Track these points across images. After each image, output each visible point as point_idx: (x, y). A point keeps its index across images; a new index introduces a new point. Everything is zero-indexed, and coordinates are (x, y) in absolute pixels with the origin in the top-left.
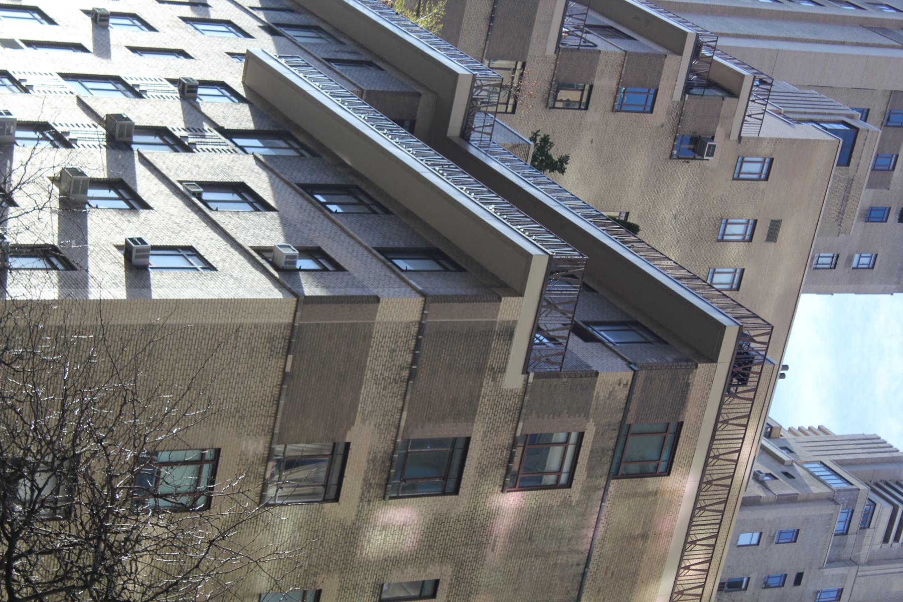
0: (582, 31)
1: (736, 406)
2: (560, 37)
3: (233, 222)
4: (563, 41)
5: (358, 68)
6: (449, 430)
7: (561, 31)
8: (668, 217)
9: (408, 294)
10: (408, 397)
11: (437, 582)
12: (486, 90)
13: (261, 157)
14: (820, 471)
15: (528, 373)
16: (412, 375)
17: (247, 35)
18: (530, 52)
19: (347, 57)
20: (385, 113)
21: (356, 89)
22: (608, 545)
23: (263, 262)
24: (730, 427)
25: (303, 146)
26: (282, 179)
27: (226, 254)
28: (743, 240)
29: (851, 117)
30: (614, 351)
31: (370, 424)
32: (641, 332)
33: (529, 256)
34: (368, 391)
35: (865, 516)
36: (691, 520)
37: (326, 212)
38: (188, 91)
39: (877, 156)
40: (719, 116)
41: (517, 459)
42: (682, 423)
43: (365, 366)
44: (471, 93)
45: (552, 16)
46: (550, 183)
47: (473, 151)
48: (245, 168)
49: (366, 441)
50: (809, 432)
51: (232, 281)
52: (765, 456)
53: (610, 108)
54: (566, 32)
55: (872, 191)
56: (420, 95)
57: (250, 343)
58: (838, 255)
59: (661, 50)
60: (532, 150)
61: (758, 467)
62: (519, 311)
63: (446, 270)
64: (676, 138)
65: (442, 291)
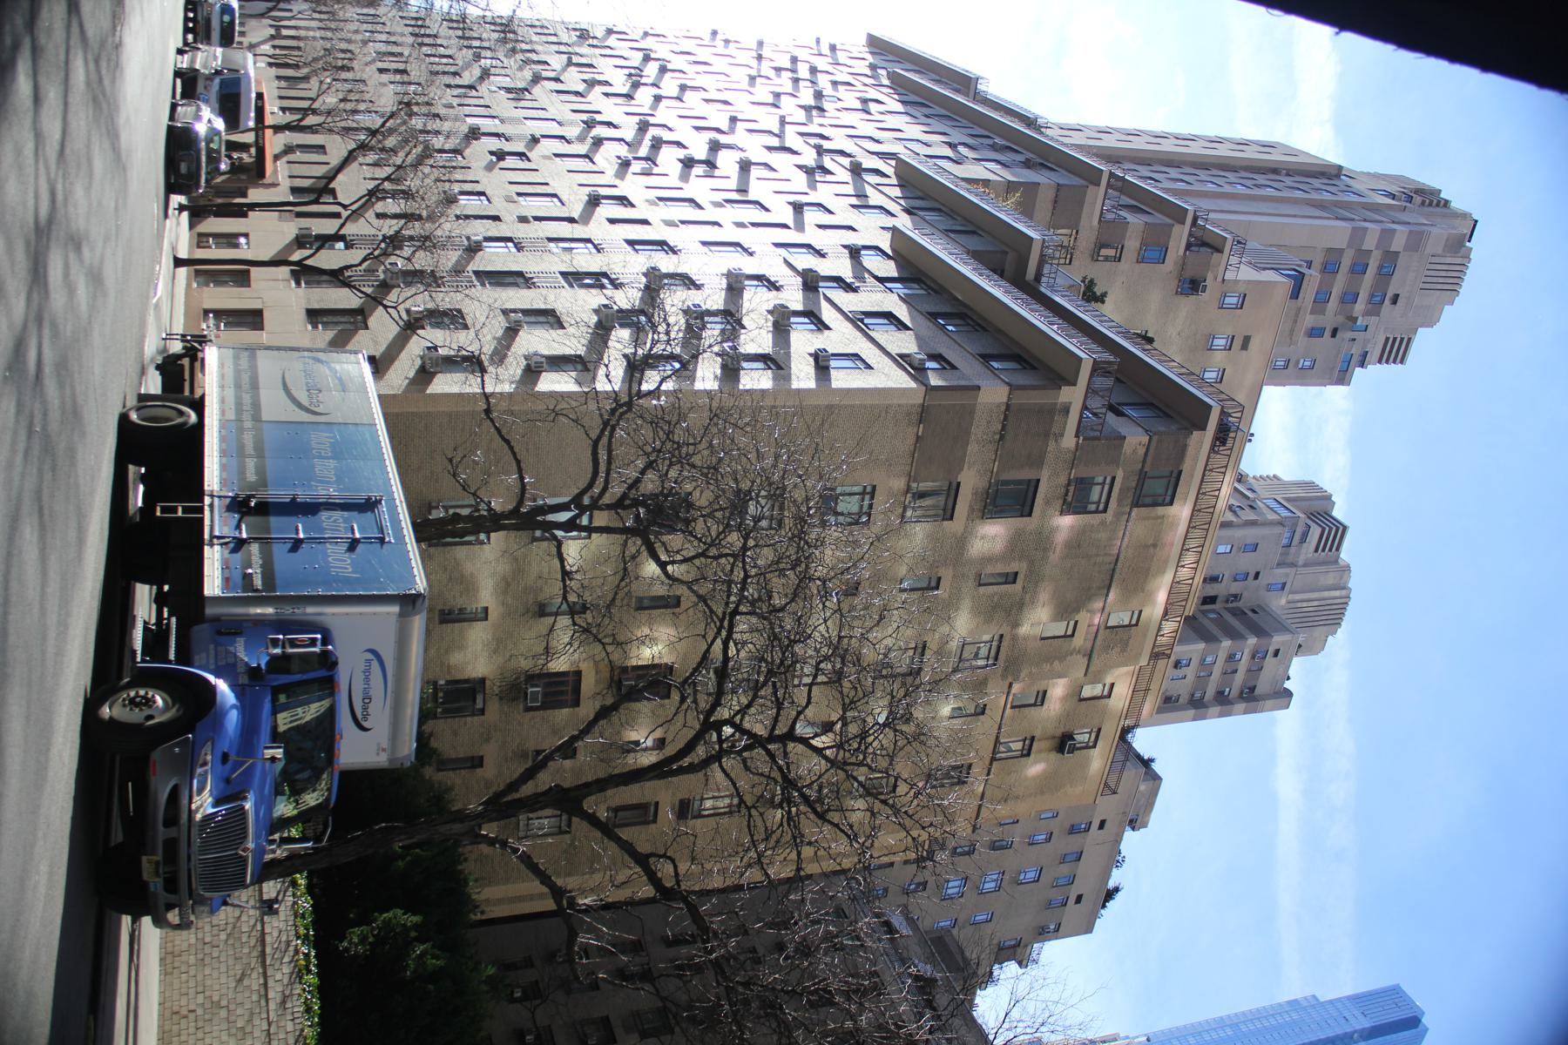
6: (1026, 474)
16: (1002, 438)
33: (1080, 359)
34: (973, 448)
38: (854, 252)
49: (971, 481)
61: (1232, 501)
62: (1072, 396)
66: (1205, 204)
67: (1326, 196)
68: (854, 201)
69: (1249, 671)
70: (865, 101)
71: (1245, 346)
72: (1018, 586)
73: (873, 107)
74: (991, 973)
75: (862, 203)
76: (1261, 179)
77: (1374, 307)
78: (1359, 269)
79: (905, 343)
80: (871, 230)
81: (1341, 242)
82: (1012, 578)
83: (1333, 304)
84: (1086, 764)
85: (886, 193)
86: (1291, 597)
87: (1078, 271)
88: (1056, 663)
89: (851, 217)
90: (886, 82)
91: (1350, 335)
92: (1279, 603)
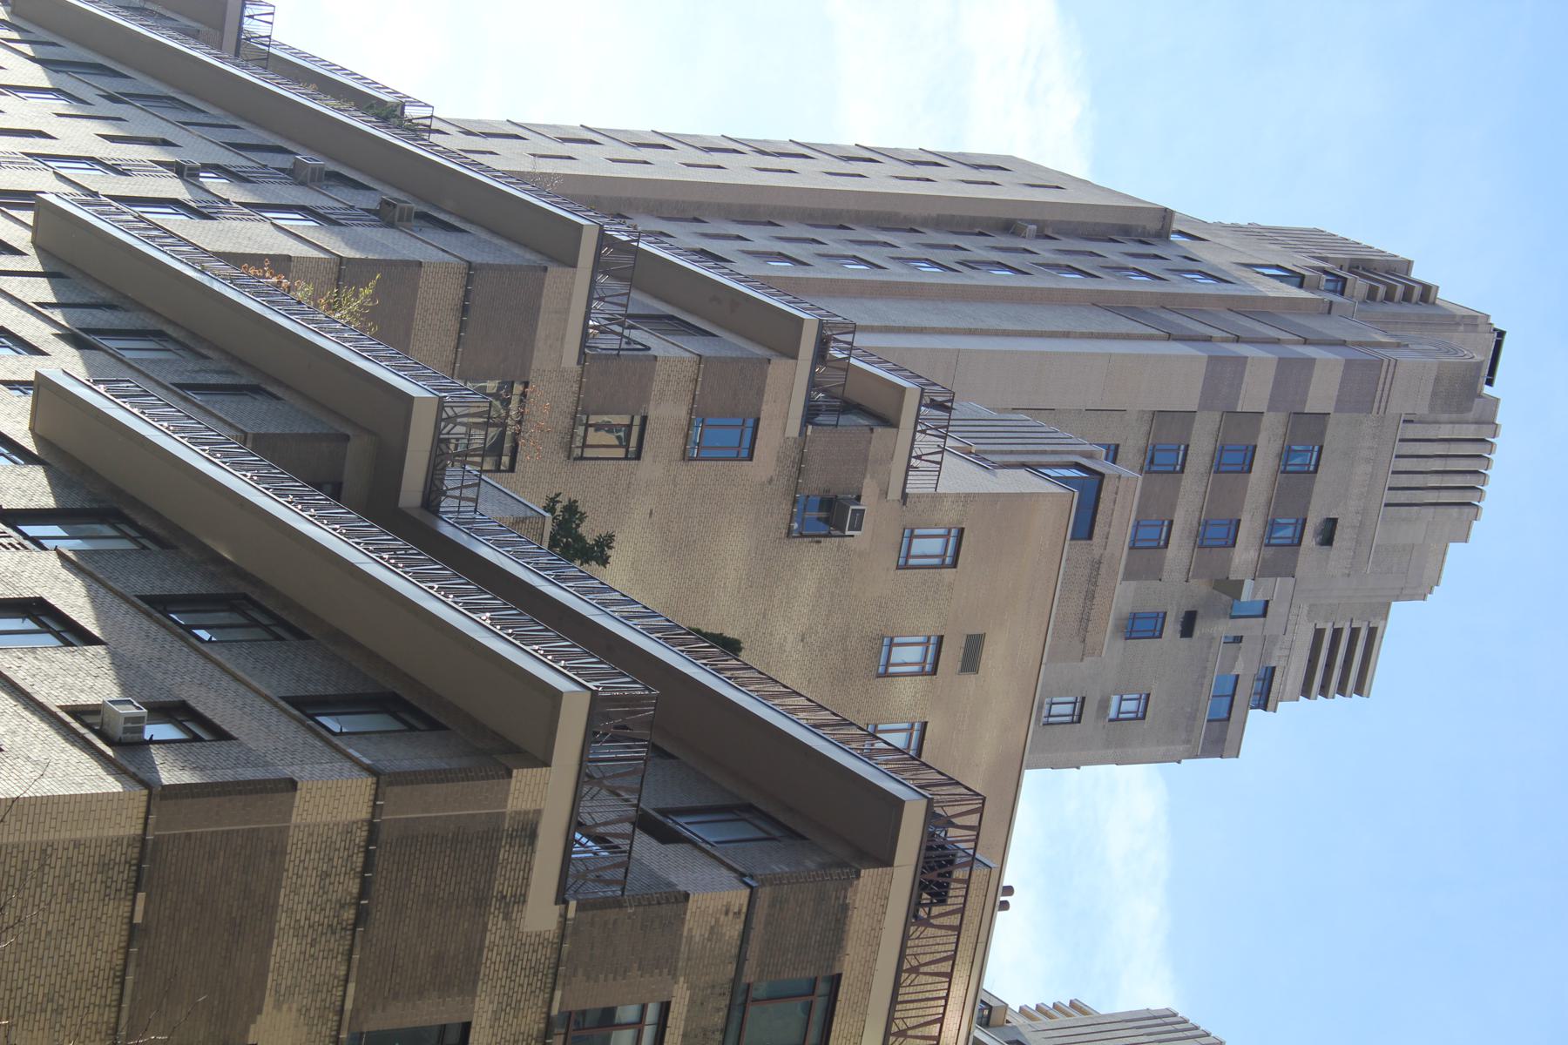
0: (621, 325)
1: (931, 941)
2: (585, 335)
3: (25, 666)
4: (590, 343)
5: (236, 398)
7: (586, 326)
8: (790, 638)
9: (346, 773)
10: (356, 957)
12: (461, 424)
13: (70, 554)
15: (566, 903)
16: (362, 916)
17: (34, 350)
18: (535, 364)
19: (213, 379)
20: (286, 467)
21: (233, 433)
23: (83, 731)
24: (923, 979)
25: (145, 533)
26: (111, 589)
27: (16, 721)
28: (922, 673)
30: (714, 857)
31: (290, 1009)
32: (757, 822)
33: (556, 695)
34: (285, 949)
37: (192, 640)
39: (1137, 525)
40: (866, 460)
42: (839, 976)
43: (276, 905)
45: (569, 300)
46: (584, 578)
47: (446, 530)
50: (1054, 1013)
51: (30, 767)
53: (678, 455)
54: (594, 327)
55: (1133, 584)
56: (347, 438)
57: (67, 875)
58: (1084, 699)
59: (759, 351)
60: (548, 528)
62: (544, 792)
63: (412, 728)
64: (795, 501)
65: (406, 765)
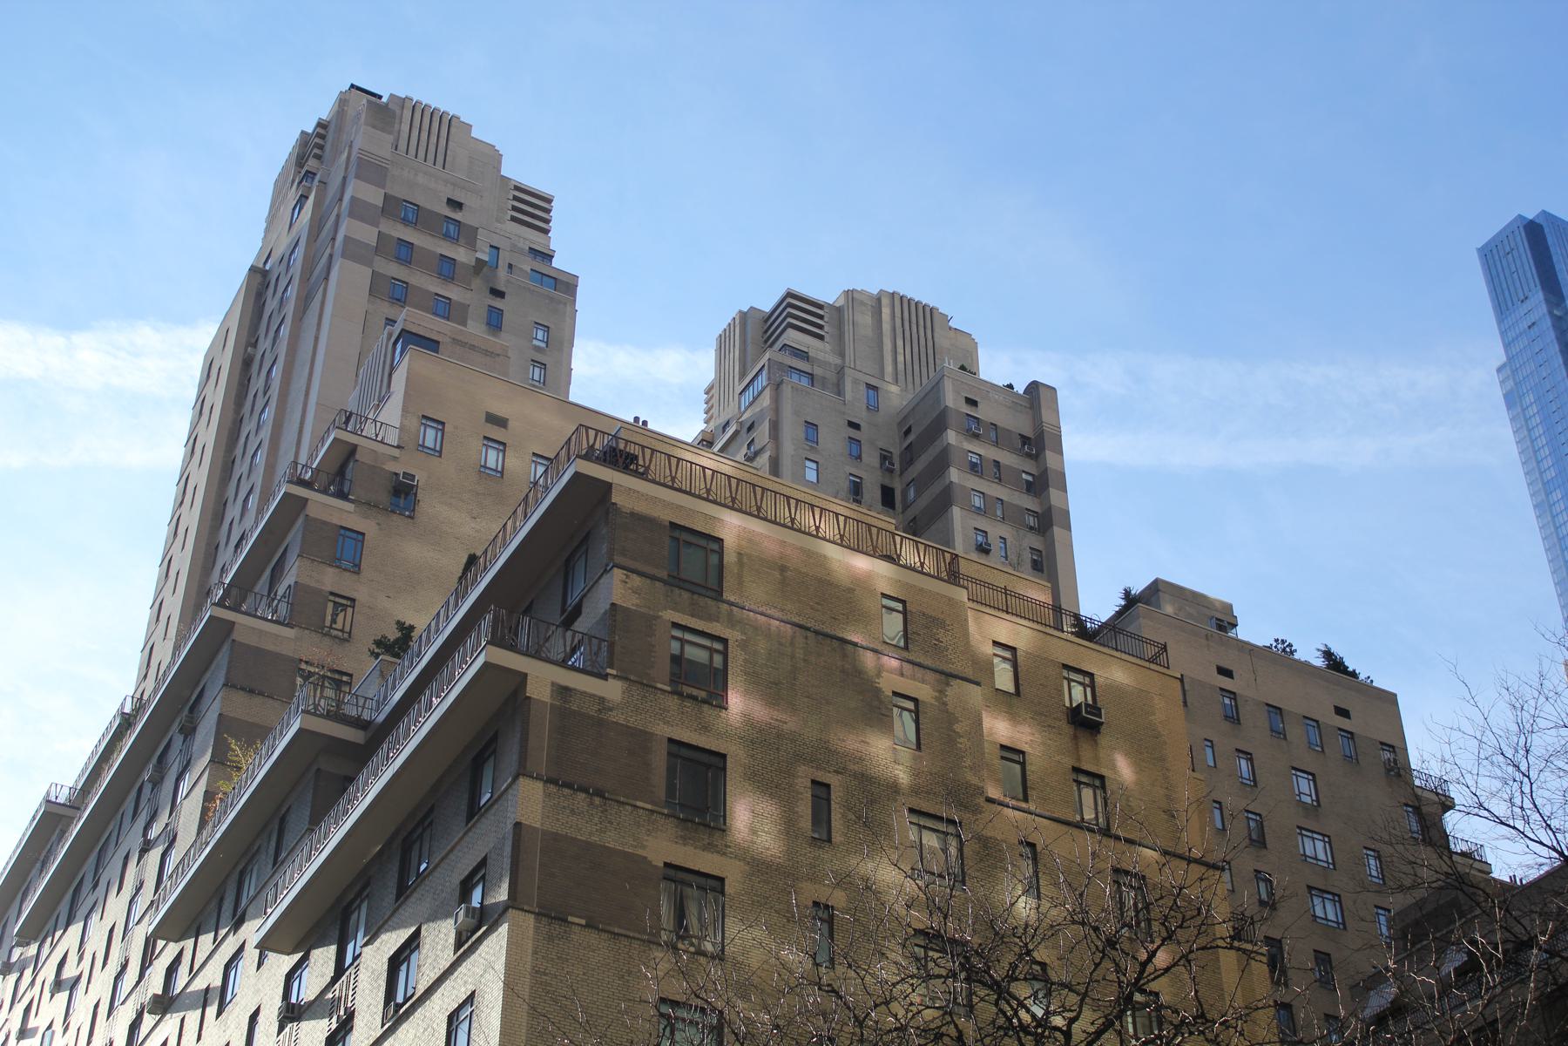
2: (277, 622)
6: (659, 759)
7: (271, 621)
11: (813, 782)
14: (749, 396)
16: (599, 793)
17: (241, 948)
22: (789, 607)
25: (359, 894)
29: (390, 335)
33: (486, 665)
34: (612, 840)
35: (796, 355)
36: (685, 492)
38: (292, 1013)
41: (695, 692)
42: (671, 523)
43: (587, 843)
44: (321, 716)
47: (381, 718)
48: (374, 956)
49: (663, 846)
52: (731, 449)
61: (740, 457)
62: (542, 679)
63: (494, 751)
65: (515, 757)
66: (283, 467)
67: (292, 292)
68: (212, 1010)
69: (996, 444)
70: (58, 985)
71: (501, 422)
72: (833, 780)
73: (69, 972)
74: (1463, 854)
75: (220, 997)
76: (257, 384)
77: (463, 234)
78: (405, 253)
79: (440, 939)
80: (261, 985)
81: (362, 275)
82: (821, 790)
83: (454, 293)
84: (1117, 690)
85: (206, 959)
86: (888, 378)
87: (360, 663)
88: (957, 727)
89: (238, 1015)
90: (32, 950)
91: (502, 273)
92: (896, 396)
